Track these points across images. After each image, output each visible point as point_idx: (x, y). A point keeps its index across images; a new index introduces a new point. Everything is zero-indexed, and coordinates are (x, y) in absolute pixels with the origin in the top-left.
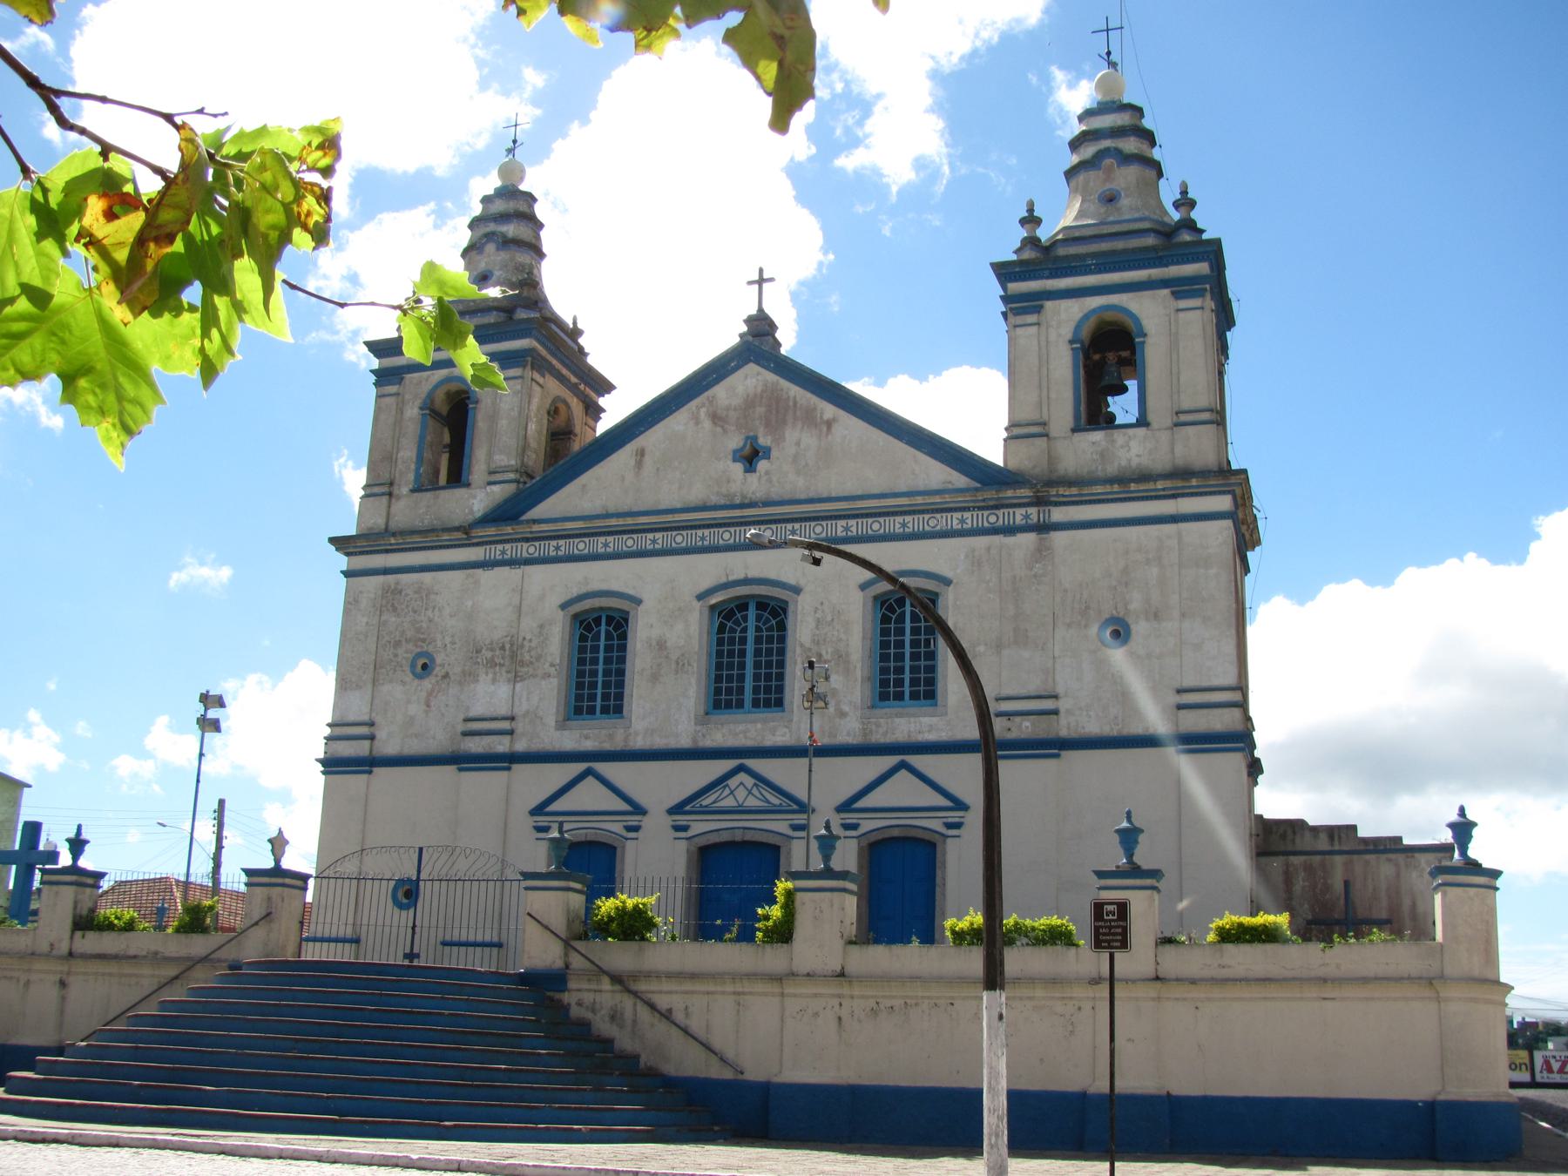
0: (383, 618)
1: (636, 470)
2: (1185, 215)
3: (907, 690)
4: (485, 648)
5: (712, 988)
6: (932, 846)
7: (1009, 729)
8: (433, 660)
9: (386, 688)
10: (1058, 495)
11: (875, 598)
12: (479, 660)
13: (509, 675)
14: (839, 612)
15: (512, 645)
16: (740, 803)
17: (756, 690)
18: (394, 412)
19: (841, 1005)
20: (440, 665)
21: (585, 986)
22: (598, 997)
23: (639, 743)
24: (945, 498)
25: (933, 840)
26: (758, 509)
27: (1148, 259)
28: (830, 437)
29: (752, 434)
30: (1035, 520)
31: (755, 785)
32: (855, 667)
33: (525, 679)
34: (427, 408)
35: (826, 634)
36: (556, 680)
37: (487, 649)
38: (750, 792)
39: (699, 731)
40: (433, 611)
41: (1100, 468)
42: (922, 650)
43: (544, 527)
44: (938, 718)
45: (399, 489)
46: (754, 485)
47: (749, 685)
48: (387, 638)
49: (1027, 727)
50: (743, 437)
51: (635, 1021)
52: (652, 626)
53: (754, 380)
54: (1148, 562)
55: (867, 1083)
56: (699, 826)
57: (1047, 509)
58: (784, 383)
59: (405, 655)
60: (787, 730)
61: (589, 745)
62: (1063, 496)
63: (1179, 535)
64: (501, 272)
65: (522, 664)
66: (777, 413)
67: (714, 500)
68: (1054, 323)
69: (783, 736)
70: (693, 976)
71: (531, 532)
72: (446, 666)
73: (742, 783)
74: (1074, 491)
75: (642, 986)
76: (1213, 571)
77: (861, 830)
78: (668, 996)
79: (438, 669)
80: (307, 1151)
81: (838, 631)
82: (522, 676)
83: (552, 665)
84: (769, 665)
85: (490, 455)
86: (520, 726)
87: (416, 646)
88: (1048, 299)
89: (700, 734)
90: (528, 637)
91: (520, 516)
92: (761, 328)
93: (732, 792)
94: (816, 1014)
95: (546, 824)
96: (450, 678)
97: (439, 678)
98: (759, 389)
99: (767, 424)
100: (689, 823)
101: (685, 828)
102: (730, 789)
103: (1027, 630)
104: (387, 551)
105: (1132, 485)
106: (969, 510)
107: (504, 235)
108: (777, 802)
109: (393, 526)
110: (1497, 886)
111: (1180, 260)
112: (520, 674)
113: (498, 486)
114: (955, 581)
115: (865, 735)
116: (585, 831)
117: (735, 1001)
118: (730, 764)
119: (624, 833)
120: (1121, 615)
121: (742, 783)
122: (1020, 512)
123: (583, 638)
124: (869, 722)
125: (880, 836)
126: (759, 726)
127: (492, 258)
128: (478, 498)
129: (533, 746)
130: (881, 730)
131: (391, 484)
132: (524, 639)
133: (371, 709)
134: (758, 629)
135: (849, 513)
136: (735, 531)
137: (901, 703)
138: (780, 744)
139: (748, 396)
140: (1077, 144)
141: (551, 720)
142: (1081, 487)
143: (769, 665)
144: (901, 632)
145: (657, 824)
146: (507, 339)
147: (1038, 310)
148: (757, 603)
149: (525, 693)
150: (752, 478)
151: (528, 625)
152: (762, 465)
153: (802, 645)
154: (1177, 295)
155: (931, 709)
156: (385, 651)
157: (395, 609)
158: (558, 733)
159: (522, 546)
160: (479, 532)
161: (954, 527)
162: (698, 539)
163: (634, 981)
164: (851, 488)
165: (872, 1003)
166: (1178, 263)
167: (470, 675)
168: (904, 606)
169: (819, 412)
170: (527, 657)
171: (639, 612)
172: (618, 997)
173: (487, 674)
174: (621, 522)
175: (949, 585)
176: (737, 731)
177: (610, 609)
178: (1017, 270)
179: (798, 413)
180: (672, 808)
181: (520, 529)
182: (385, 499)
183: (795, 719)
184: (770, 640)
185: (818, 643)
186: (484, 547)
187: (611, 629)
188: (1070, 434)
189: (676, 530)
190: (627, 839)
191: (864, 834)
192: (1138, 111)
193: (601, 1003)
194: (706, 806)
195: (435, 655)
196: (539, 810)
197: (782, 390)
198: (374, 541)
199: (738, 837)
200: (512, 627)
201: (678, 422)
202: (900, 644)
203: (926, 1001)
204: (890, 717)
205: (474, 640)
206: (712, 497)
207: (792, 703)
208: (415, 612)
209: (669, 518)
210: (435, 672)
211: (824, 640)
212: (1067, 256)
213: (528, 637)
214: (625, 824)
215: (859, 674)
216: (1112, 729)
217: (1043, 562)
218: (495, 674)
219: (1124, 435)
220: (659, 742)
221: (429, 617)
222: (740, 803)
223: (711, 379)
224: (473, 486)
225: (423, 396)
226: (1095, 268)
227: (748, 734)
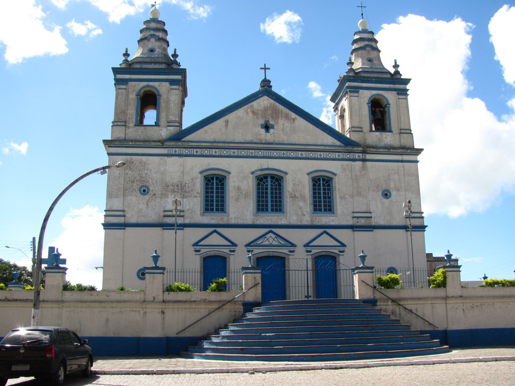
0: (126, 171)
1: (226, 127)
2: (175, 59)
3: (323, 208)
4: (170, 185)
5: (424, 302)
6: (284, 258)
7: (358, 222)
8: (148, 189)
9: (129, 198)
10: (370, 151)
11: (204, 176)
12: (168, 190)
13: (181, 196)
14: (301, 182)
15: (181, 185)
16: (271, 243)
17: (272, 205)
18: (125, 95)
19: (463, 305)
20: (151, 191)
21: (383, 304)
22: (387, 307)
23: (233, 222)
24: (335, 148)
25: (335, 256)
26: (274, 145)
27: (146, 72)
28: (294, 124)
29: (267, 120)
30: (362, 158)
31: (276, 237)
32: (307, 200)
33: (187, 198)
34: (139, 96)
35: (297, 189)
36: (199, 198)
37: (171, 186)
38: (274, 239)
39: (255, 219)
40: (147, 171)
41: (379, 143)
42: (327, 195)
43: (194, 144)
44: (335, 218)
45: (129, 124)
46: (269, 137)
47: (269, 204)
48: (128, 179)
49: (363, 222)
50: (264, 120)
51: (400, 314)
52: (235, 182)
53: (267, 102)
54: (395, 173)
55: (473, 328)
56: (257, 251)
57: (365, 154)
58: (277, 104)
59: (136, 186)
60: (285, 219)
61: (213, 222)
62: (372, 151)
63: (403, 166)
64: (159, 50)
65: (185, 192)
66: (276, 114)
67: (255, 140)
68: (362, 97)
69: (284, 221)
70: (419, 299)
71: (188, 145)
72: (154, 191)
73: (271, 236)
74: (375, 150)
75: (401, 303)
76: (413, 178)
77: (312, 253)
78: (410, 305)
79: (151, 192)
80: (443, 361)
81: (301, 188)
82: (186, 196)
83: (197, 193)
84: (276, 197)
85: (167, 116)
86: (186, 214)
87: (141, 183)
88: (360, 89)
89: (255, 219)
90: (187, 182)
91: (181, 139)
92: (266, 84)
93: (267, 239)
94: (457, 309)
95: (199, 249)
96: (156, 196)
97: (152, 195)
98: (269, 105)
99: (272, 117)
100: (200, 249)
101: (199, 251)
102: (267, 239)
103: (361, 192)
104: (127, 147)
105: (392, 150)
106: (341, 152)
107: (158, 36)
108: (283, 243)
109: (127, 137)
110: (460, 270)
111: (138, 73)
112: (185, 196)
113: (172, 127)
114: (337, 175)
115: (312, 222)
116: (214, 252)
117: (431, 306)
118: (267, 230)
119: (229, 253)
120: (388, 189)
121: (271, 236)
122: (357, 155)
123: (207, 184)
124: (313, 218)
125: (318, 255)
126: (276, 218)
127: (154, 44)
128: (163, 131)
129: (192, 221)
130: (317, 221)
131: (126, 122)
132: (186, 183)
133: (123, 206)
134: (271, 185)
135: (209, 147)
136: (190, 150)
137: (321, 212)
138: (284, 224)
139: (265, 106)
140: (357, 41)
141: (198, 212)
142: (375, 149)
143: (276, 197)
144: (320, 189)
145: (241, 250)
146: (172, 75)
147: (358, 92)
148: (271, 176)
149: (187, 202)
150: (268, 135)
151: (187, 179)
152: (271, 131)
153: (289, 192)
154: (398, 94)
155: (333, 214)
156: (127, 184)
157: (131, 169)
158: (201, 217)
159: (183, 150)
160: (168, 143)
161: (299, 156)
162: (250, 153)
163: (399, 301)
164: (302, 141)
165: (471, 304)
166: (399, 84)
167: (164, 195)
168: (320, 181)
169: (290, 115)
170: (187, 190)
171: (230, 177)
172: (394, 307)
173: (172, 195)
174: (224, 145)
175: (336, 176)
176: (268, 219)
177: (218, 175)
178: (352, 78)
179: (283, 115)
180: (194, 244)
181: (180, 144)
182: (124, 127)
183: (288, 216)
184: (276, 189)
185: (294, 191)
186: (168, 149)
187: (272, 184)
188: (369, 132)
189: (242, 150)
190: (230, 255)
191: (313, 254)
192: (164, 24)
193: (388, 309)
194: (259, 244)
195: (149, 187)
196: (196, 244)
197: (277, 106)
198: (122, 143)
199: (271, 254)
200: (181, 178)
201: (240, 112)
202: (320, 193)
203: (487, 303)
204: (319, 217)
205: (165, 182)
206: (255, 140)
207: (287, 211)
208: (139, 170)
209: (242, 145)
210: (150, 193)
211: (296, 190)
212: (367, 77)
213: (187, 182)
214: (339, 250)
215: (308, 202)
216: (387, 223)
217: (364, 171)
218: (175, 195)
219: (385, 134)
220: (240, 222)
221: (146, 173)
222: (271, 243)
223: (253, 99)
224: (161, 126)
225: (137, 91)
226: (374, 82)
227: (272, 220)
